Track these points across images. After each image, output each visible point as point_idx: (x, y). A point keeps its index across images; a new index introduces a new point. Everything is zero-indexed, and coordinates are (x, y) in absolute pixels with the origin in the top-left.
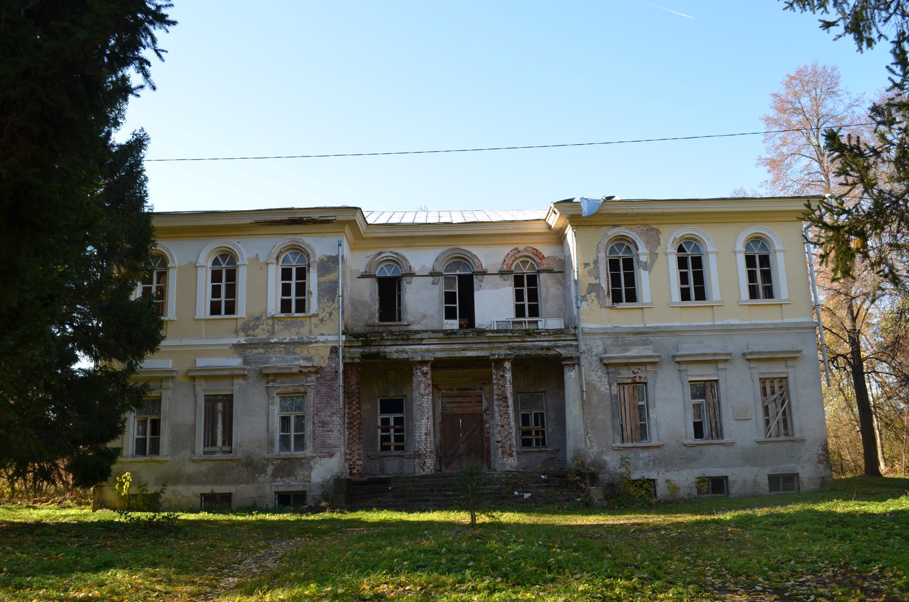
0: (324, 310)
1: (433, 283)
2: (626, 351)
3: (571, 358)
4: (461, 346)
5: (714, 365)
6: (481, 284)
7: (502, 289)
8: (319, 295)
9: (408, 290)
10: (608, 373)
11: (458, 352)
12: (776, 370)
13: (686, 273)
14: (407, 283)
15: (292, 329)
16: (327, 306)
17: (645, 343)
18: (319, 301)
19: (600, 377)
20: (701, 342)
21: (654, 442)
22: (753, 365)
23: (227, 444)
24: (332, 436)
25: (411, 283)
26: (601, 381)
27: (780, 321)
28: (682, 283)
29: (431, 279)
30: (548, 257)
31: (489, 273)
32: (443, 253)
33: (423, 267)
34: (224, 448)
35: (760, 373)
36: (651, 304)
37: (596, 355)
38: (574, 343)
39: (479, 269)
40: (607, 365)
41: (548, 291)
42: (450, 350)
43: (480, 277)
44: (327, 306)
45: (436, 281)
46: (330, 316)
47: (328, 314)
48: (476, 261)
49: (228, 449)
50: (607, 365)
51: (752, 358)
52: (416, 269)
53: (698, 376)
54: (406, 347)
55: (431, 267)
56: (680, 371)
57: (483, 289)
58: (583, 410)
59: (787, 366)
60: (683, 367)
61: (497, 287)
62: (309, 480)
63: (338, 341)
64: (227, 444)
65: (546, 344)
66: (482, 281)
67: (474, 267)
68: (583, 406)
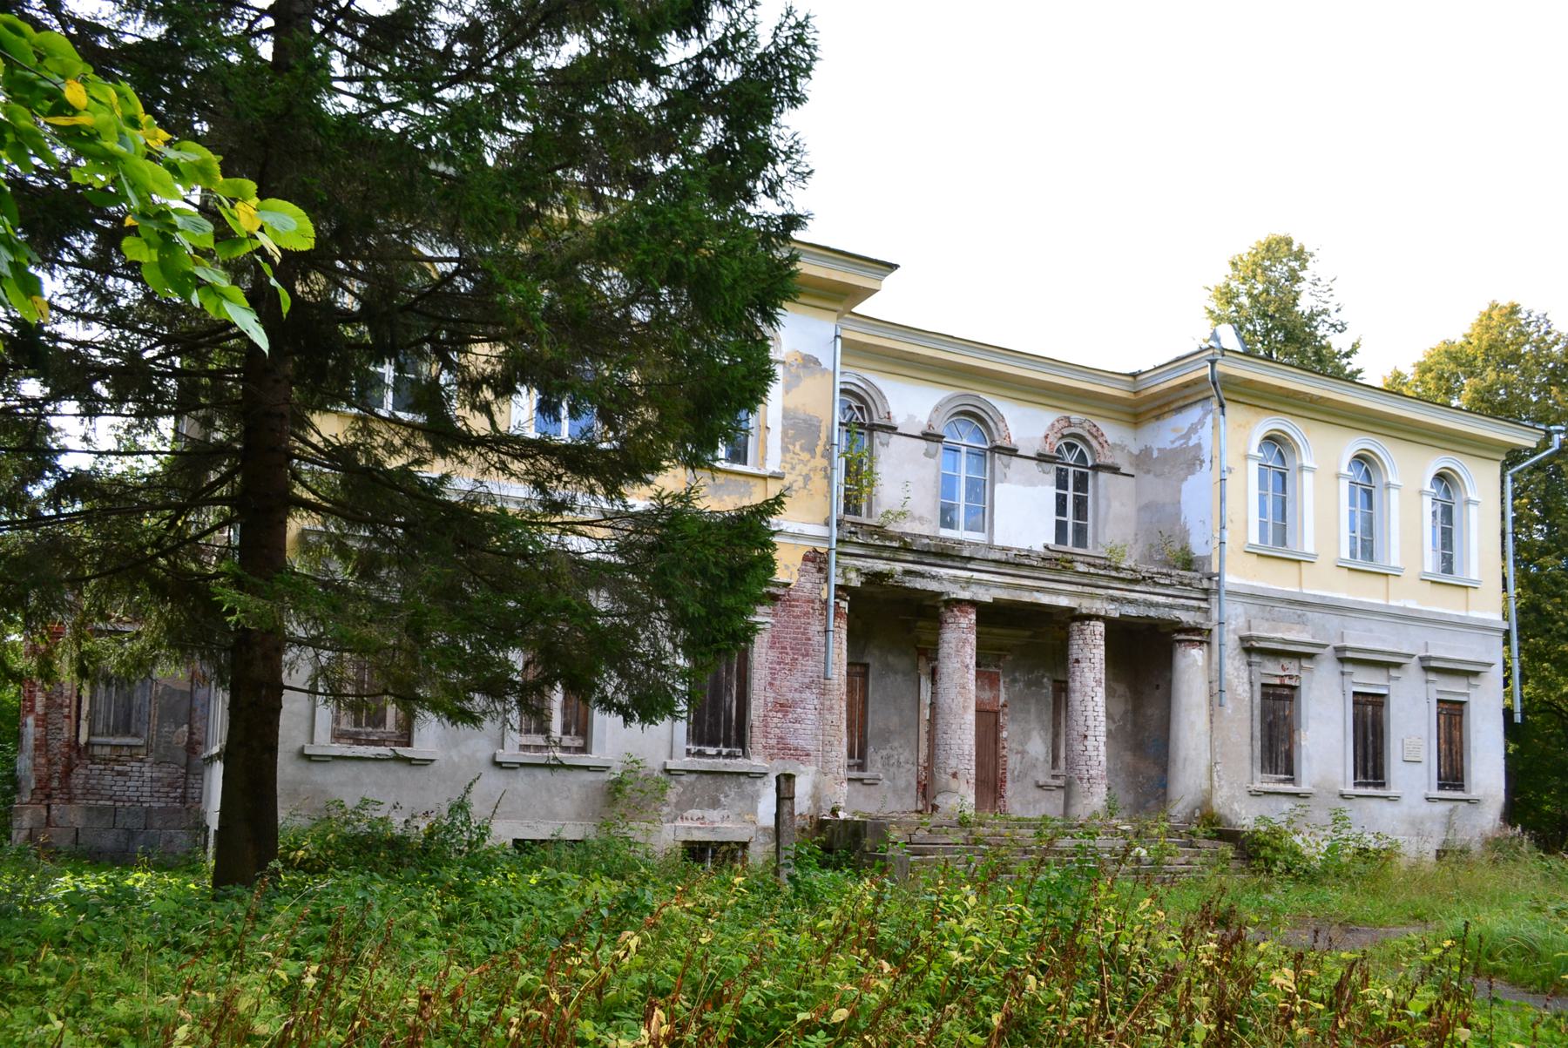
0: (793, 468)
1: (927, 454)
2: (1275, 630)
3: (1196, 630)
4: (1170, 600)
5: (1384, 672)
6: (1007, 470)
7: (1040, 487)
8: (785, 433)
9: (882, 458)
10: (1250, 664)
11: (1266, 625)
12: (1454, 688)
13: (1065, 496)
14: (882, 444)
15: (725, 497)
16: (801, 461)
17: (1302, 621)
18: (785, 450)
19: (1237, 669)
20: (1371, 631)
21: (1304, 787)
22: (1432, 677)
23: (573, 730)
24: (801, 732)
25: (887, 445)
26: (1238, 677)
27: (1463, 613)
28: (1058, 513)
29: (923, 443)
30: (1538, 444)
31: (1019, 453)
32: (950, 400)
33: (911, 417)
34: (567, 741)
35: (1438, 691)
36: (1315, 556)
37: (1235, 631)
38: (1203, 605)
39: (1005, 444)
40: (1251, 649)
41: (1109, 506)
42: (1171, 607)
43: (1005, 458)
44: (801, 461)
45: (932, 451)
46: (805, 484)
47: (801, 478)
48: (1001, 425)
49: (579, 742)
50: (1251, 649)
51: (1431, 668)
52: (898, 420)
53: (1365, 685)
54: (942, 571)
55: (925, 422)
56: (1343, 673)
57: (1010, 482)
58: (1211, 722)
59: (1390, 678)
60: (1348, 668)
61: (1031, 483)
62: (753, 818)
63: (827, 539)
64: (573, 730)
65: (1162, 599)
66: (1007, 466)
67: (997, 437)
68: (1211, 715)
